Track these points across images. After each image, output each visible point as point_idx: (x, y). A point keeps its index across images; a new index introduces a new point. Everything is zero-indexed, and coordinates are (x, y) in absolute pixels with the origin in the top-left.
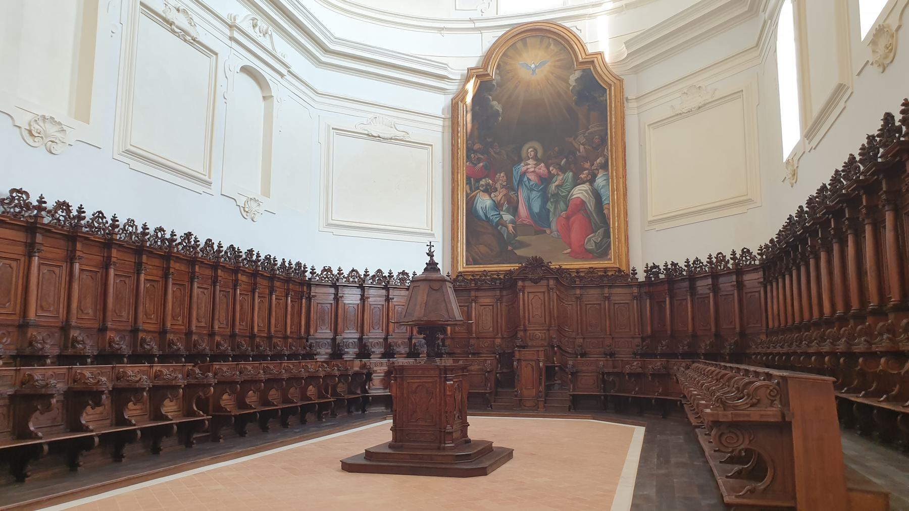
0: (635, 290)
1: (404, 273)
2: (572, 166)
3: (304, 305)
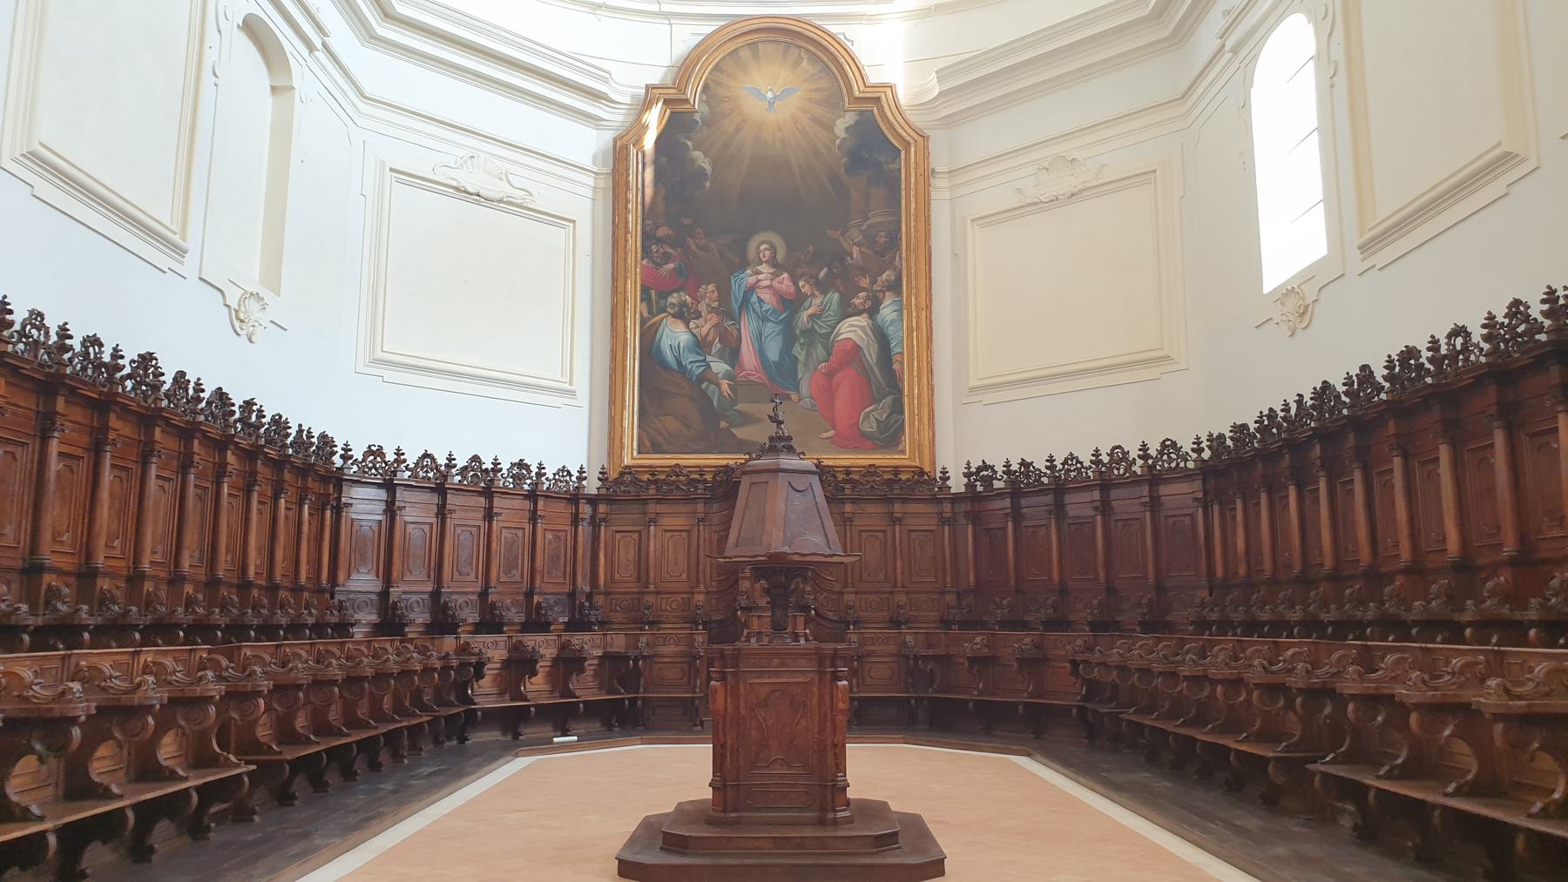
0: (947, 507)
1: (521, 464)
2: (839, 282)
3: (328, 522)
